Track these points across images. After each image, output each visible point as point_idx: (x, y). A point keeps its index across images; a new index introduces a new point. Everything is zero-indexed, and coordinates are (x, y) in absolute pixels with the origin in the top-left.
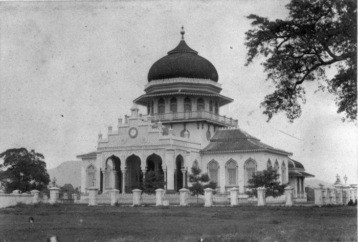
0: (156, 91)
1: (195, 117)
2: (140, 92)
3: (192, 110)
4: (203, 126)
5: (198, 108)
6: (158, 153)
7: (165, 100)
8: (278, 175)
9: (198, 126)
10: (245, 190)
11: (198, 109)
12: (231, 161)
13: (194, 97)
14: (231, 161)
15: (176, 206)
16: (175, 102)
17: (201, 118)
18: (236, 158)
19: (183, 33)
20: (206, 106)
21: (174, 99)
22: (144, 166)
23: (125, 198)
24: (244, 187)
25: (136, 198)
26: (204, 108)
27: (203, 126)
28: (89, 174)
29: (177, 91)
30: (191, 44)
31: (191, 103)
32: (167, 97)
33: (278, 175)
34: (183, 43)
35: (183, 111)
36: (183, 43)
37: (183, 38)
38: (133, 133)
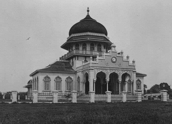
2: (65, 41)
4: (78, 58)
5: (91, 49)
7: (80, 45)
11: (83, 50)
12: (58, 77)
14: (58, 77)
15: (117, 102)
18: (61, 76)
19: (88, 11)
20: (87, 47)
21: (84, 45)
22: (108, 79)
23: (101, 97)
25: (109, 97)
26: (94, 49)
27: (78, 58)
28: (45, 82)
29: (87, 39)
30: (93, 16)
34: (88, 17)
35: (90, 50)
36: (88, 17)
37: (88, 13)
38: (114, 60)
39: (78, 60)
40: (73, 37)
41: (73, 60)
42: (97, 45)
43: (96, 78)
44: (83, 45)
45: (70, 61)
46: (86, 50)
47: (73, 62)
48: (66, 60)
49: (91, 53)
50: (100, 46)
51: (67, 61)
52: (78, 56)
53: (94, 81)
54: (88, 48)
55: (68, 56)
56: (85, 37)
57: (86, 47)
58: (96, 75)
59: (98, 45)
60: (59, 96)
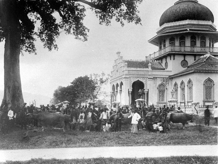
0: (168, 31)
1: (188, 51)
3: (176, 45)
4: (174, 57)
6: (141, 80)
8: (11, 91)
9: (171, 57)
10: (204, 103)
11: (180, 45)
13: (198, 34)
16: (174, 41)
17: (181, 52)
24: (203, 101)
26: (195, 44)
27: (174, 57)
31: (175, 41)
32: (177, 35)
33: (11, 91)
39: (174, 59)
40: (165, 28)
41: (166, 61)
42: (200, 37)
43: (132, 88)
44: (192, 38)
45: (162, 61)
46: (174, 45)
47: (166, 62)
48: (156, 60)
49: (202, 49)
50: (195, 38)
51: (157, 61)
52: (174, 55)
53: (129, 92)
54: (188, 42)
55: (154, 56)
56: (184, 28)
57: (185, 42)
58: (131, 85)
59: (191, 37)
60: (159, 103)
